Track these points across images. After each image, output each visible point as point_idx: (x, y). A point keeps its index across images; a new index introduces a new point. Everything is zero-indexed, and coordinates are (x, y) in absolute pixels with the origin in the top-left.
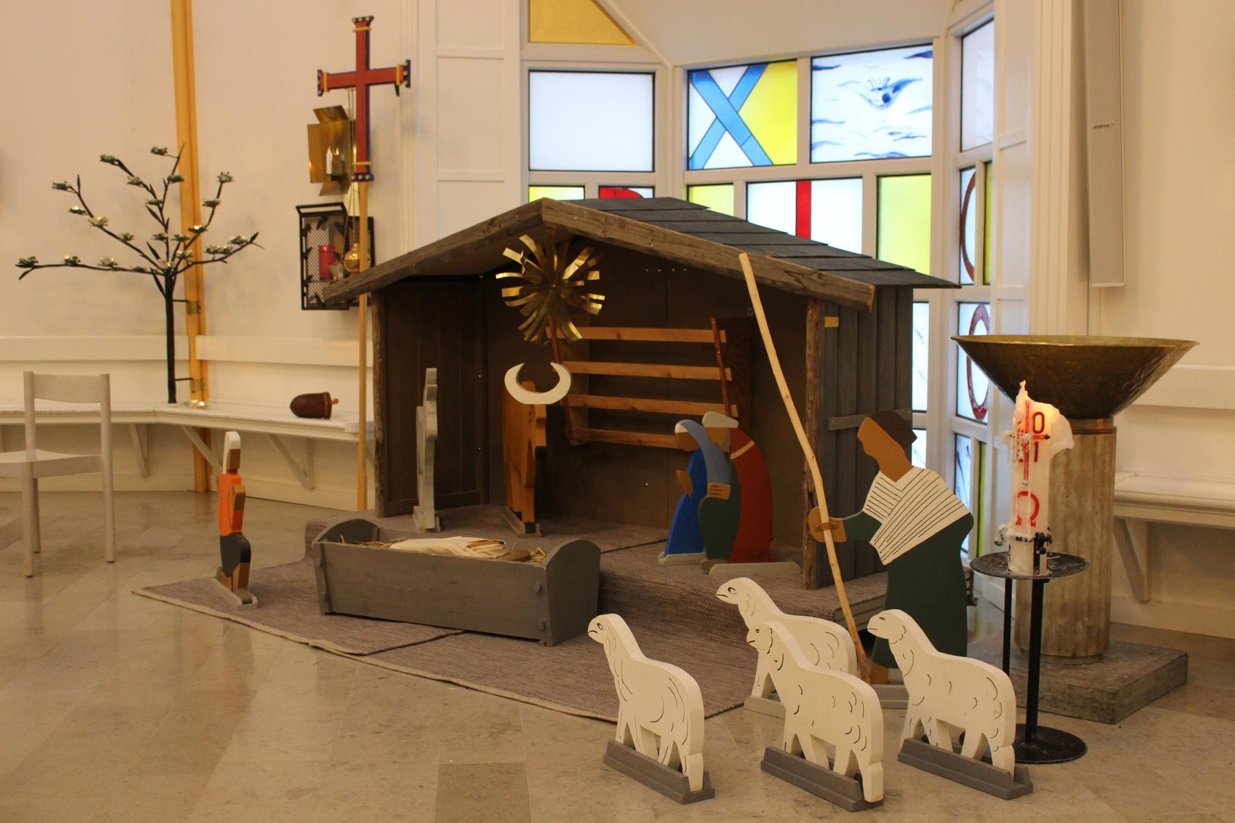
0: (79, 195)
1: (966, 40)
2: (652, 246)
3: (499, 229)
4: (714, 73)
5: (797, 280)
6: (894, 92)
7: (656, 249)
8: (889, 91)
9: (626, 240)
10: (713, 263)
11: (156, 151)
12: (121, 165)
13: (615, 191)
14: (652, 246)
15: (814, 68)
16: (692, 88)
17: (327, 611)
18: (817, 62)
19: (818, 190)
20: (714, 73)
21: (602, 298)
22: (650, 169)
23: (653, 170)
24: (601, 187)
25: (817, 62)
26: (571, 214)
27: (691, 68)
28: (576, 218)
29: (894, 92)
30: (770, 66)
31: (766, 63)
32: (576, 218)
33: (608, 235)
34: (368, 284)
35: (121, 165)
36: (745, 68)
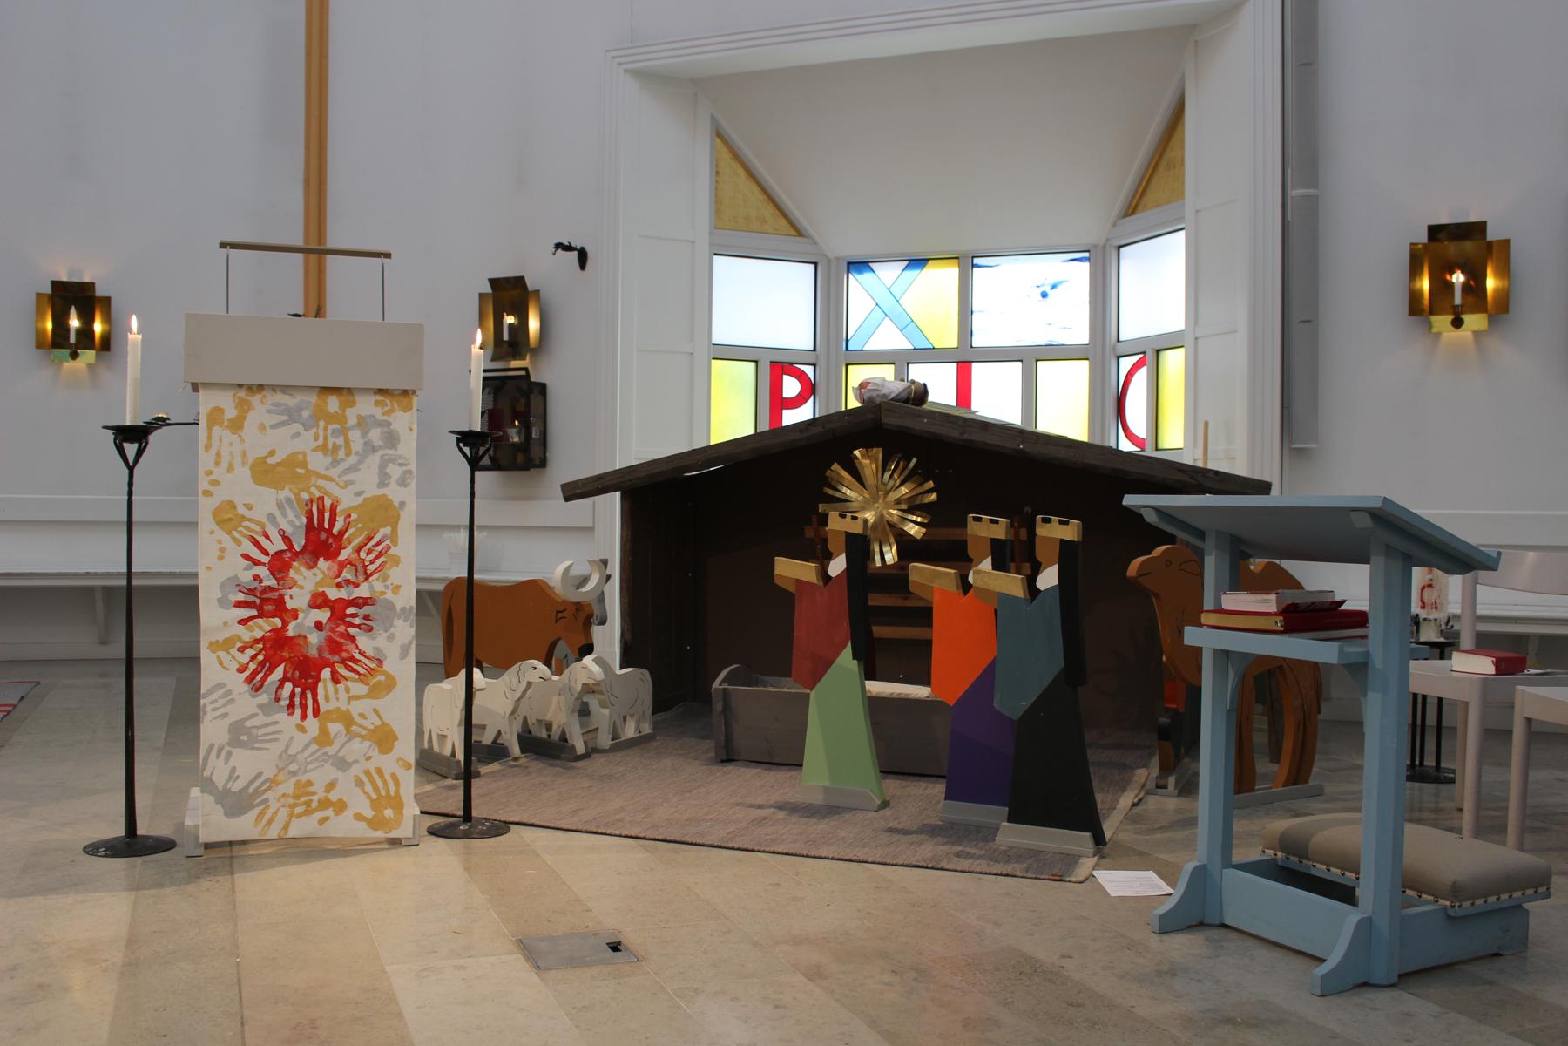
0: (131, 470)
1: (1122, 250)
2: (1021, 447)
3: (821, 430)
4: (873, 266)
5: (1192, 478)
6: (1051, 289)
7: (1027, 450)
8: (1047, 289)
9: (989, 442)
10: (1094, 462)
11: (345, 391)
12: (1081, 882)
13: (782, 367)
14: (1021, 447)
15: (973, 266)
16: (850, 275)
17: (725, 759)
18: (976, 261)
19: (977, 368)
20: (873, 266)
21: (930, 484)
22: (812, 348)
23: (815, 349)
24: (771, 362)
25: (976, 261)
26: (919, 416)
27: (850, 261)
28: (925, 421)
29: (1051, 289)
30: (931, 262)
31: (928, 260)
32: (925, 421)
33: (966, 437)
34: (630, 480)
35: (1081, 882)
36: (906, 263)
